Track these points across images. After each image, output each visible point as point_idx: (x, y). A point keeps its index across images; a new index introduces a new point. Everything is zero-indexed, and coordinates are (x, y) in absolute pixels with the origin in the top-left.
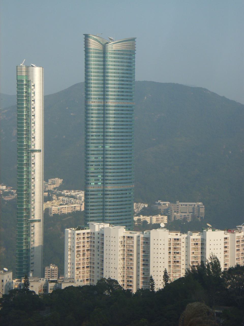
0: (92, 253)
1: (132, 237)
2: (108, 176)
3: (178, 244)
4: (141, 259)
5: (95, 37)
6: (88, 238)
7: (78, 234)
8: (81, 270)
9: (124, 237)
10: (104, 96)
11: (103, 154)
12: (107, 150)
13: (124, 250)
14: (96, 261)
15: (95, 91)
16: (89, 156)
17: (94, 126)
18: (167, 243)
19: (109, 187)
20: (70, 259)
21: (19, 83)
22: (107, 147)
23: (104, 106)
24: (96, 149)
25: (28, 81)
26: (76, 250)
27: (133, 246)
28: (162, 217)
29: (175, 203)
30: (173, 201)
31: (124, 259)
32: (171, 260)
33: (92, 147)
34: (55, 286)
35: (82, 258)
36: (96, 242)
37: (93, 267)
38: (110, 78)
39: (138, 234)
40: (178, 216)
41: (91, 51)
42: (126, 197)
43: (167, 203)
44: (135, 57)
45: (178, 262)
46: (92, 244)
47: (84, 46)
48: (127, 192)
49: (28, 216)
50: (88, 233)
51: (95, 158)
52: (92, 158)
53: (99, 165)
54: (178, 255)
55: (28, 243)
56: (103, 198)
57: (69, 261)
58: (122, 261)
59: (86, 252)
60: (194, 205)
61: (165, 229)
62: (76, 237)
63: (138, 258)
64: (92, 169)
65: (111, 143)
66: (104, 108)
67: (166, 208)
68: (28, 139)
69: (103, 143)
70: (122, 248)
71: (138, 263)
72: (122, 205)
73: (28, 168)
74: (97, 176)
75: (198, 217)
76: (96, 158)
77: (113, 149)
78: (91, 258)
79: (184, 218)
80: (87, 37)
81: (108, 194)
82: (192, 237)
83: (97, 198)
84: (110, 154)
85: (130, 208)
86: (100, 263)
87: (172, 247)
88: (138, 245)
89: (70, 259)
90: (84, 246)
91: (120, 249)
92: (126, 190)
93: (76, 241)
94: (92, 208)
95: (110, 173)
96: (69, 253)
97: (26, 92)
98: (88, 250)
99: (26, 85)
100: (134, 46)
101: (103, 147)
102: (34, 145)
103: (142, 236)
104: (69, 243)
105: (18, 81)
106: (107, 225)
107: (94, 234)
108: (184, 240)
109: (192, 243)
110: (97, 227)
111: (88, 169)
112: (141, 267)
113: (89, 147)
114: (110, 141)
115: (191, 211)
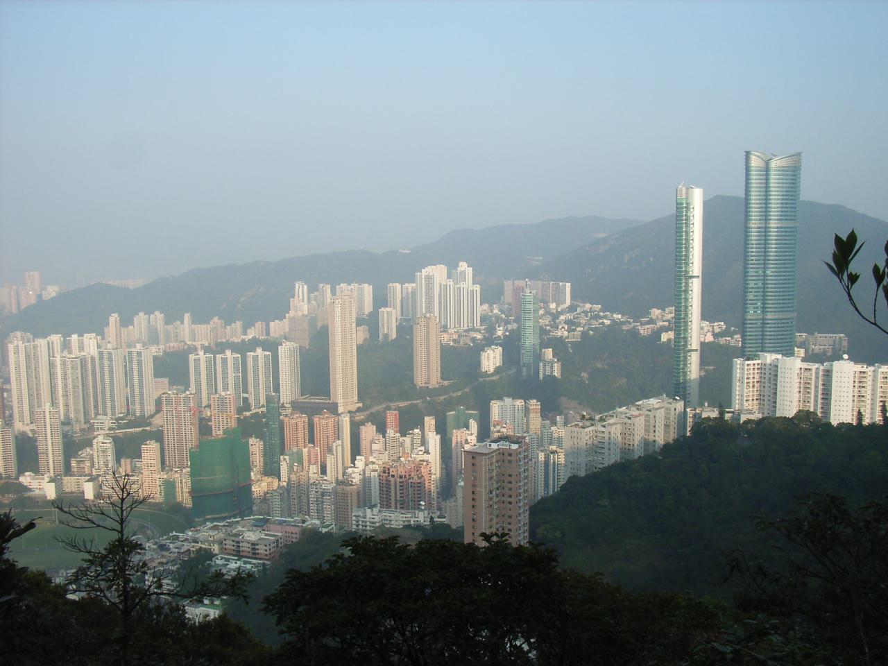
0: (762, 385)
1: (810, 369)
2: (768, 304)
3: (865, 377)
4: (820, 392)
5: (757, 154)
6: (758, 369)
7: (748, 365)
8: (750, 402)
9: (801, 369)
10: (765, 217)
11: (764, 280)
12: (768, 276)
13: (800, 383)
14: (766, 394)
15: (756, 212)
16: (747, 282)
17: (773, 246)
18: (852, 376)
19: (769, 316)
20: (739, 391)
21: (679, 206)
22: (768, 272)
23: (766, 228)
24: (757, 274)
25: (688, 204)
26: (746, 381)
27: (811, 379)
28: (798, 349)
29: (813, 334)
30: (810, 333)
31: (800, 392)
32: (856, 394)
33: (751, 272)
34: (732, 417)
35: (751, 389)
36: (767, 374)
37: (764, 400)
38: (772, 197)
39: (817, 365)
40: (817, 349)
41: (752, 169)
42: (788, 327)
43: (804, 335)
44: (800, 174)
45: (863, 396)
46: (763, 376)
47: (745, 160)
48: (790, 321)
49: (685, 346)
50: (758, 364)
51: (756, 284)
52: (752, 284)
53: (759, 292)
54: (863, 389)
55: (685, 373)
56: (763, 327)
57: (737, 393)
58: (797, 395)
59: (756, 384)
60: (836, 337)
61: (849, 361)
62: (746, 367)
63: (816, 391)
64: (751, 296)
65: (772, 268)
66: (765, 231)
67: (803, 340)
68: (687, 264)
69: (764, 268)
70: (799, 381)
71: (816, 396)
72: (783, 335)
73: (686, 295)
74: (756, 304)
75: (840, 350)
76: (756, 284)
77: (775, 274)
78: (760, 390)
79: (823, 352)
80: (748, 154)
81: (768, 324)
82: (880, 370)
83: (756, 328)
84: (772, 280)
85: (791, 338)
86: (772, 396)
87: (856, 380)
88: (817, 378)
89: (739, 391)
90: (754, 378)
91: (796, 381)
92: (788, 319)
93: (746, 372)
94: (750, 337)
95: (771, 300)
96: (738, 384)
97: (686, 215)
98: (757, 382)
99: (686, 207)
100: (799, 161)
101: (764, 272)
102: (692, 271)
103: (822, 368)
104: (737, 374)
105: (677, 204)
106: (779, 356)
107: (765, 365)
108: (870, 373)
109: (880, 376)
110: (769, 358)
111: (746, 296)
112: (820, 401)
113: (748, 272)
114: (772, 266)
115: (831, 343)
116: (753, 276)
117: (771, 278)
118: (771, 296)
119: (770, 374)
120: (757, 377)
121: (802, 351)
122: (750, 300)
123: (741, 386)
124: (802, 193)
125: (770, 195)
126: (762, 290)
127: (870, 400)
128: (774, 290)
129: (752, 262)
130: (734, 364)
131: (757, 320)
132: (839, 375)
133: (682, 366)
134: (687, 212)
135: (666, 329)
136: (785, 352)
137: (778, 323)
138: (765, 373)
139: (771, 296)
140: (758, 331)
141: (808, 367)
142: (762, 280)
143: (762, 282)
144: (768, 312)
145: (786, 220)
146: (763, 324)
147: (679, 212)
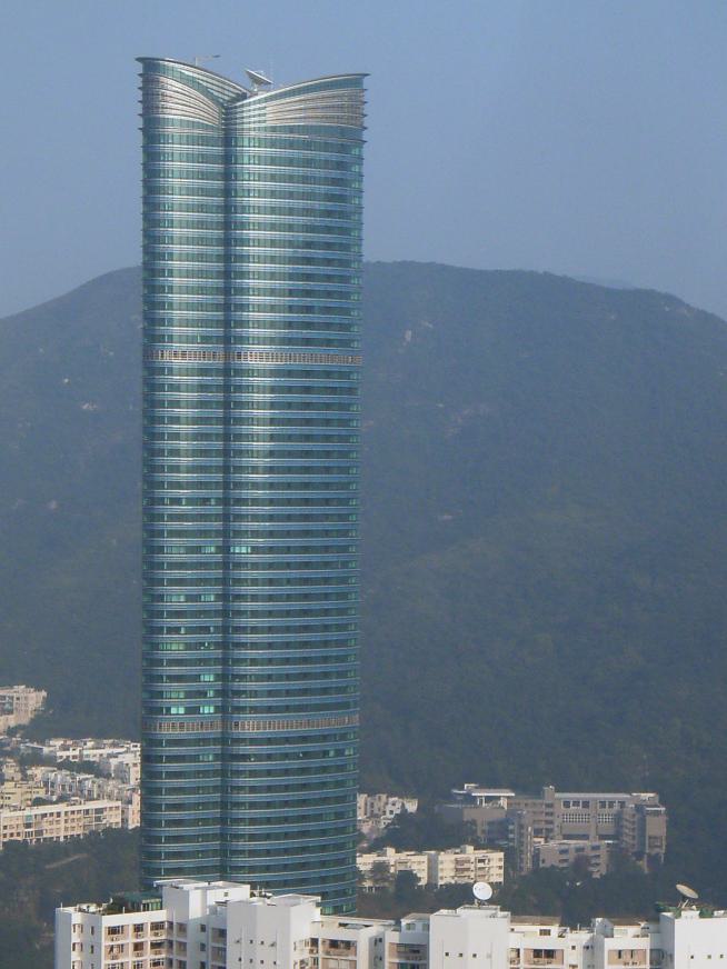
1: (348, 945)
5: (188, 72)
6: (155, 945)
7: (113, 931)
9: (314, 942)
10: (227, 328)
11: (224, 581)
12: (238, 565)
15: (189, 306)
16: (159, 589)
19: (250, 726)
22: (241, 550)
23: (226, 371)
24: (194, 557)
28: (481, 854)
29: (538, 793)
30: (528, 787)
33: (175, 550)
39: (376, 928)
40: (552, 850)
41: (170, 130)
42: (324, 769)
43: (504, 795)
44: (361, 158)
48: (329, 746)
50: (157, 926)
51: (190, 598)
52: (176, 598)
53: (206, 629)
56: (223, 773)
60: (622, 804)
61: (495, 909)
62: (105, 942)
64: (174, 646)
65: (256, 534)
66: (226, 382)
67: (499, 815)
69: (225, 533)
74: (196, 678)
75: (639, 855)
76: (190, 598)
77: (268, 558)
80: (151, 70)
81: (245, 757)
82: (610, 944)
83: (197, 774)
92: (325, 738)
94: (176, 814)
95: (254, 662)
100: (356, 109)
101: (225, 549)
103: (392, 937)
106: (240, 893)
110: (198, 899)
111: (155, 646)
113: (161, 549)
115: (609, 828)
116: (181, 566)
117: (255, 574)
119: (203, 947)
121: (496, 859)
122: (173, 662)
124: (369, 235)
125: (244, 242)
126: (219, 621)
130: (60, 926)
131: (204, 741)
139: (254, 646)
140: (205, 789)
141: (343, 935)
143: (219, 588)
145: (308, 342)
146: (226, 757)
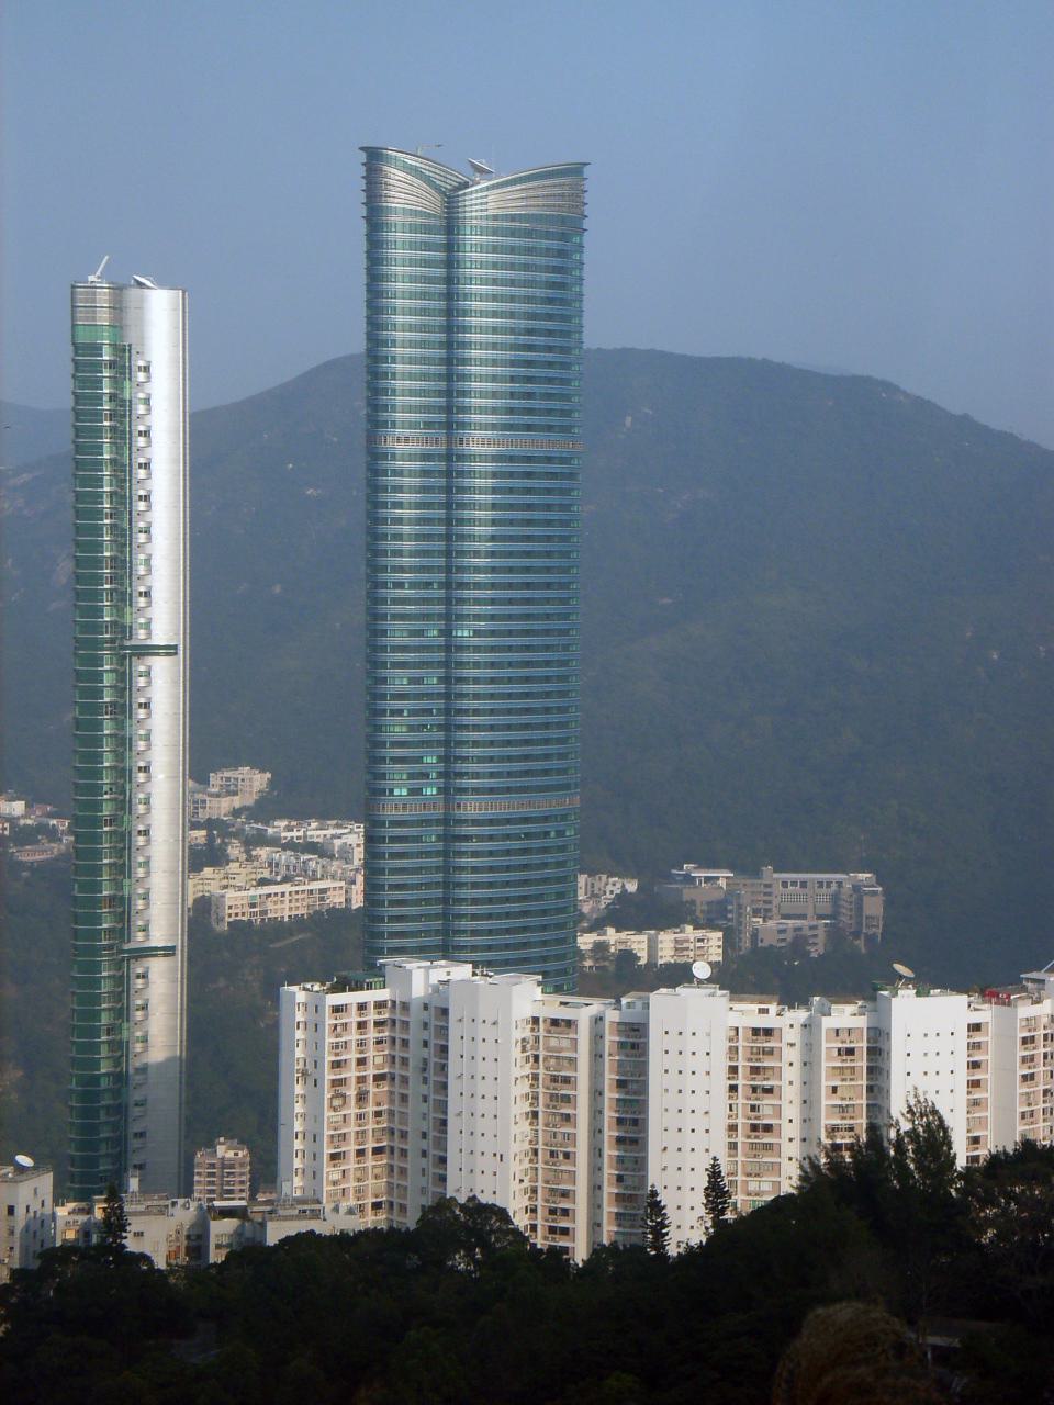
1: (569, 1023)
3: (770, 1052)
4: (609, 1114)
5: (411, 161)
6: (378, 1024)
7: (337, 1009)
8: (351, 1164)
9: (536, 1020)
10: (449, 414)
11: (446, 664)
12: (461, 648)
13: (535, 1077)
14: (413, 1126)
15: (412, 393)
16: (383, 672)
18: (720, 1047)
19: (471, 807)
21: (84, 358)
22: (463, 633)
23: (449, 457)
24: (415, 641)
25: (122, 350)
26: (329, 1076)
27: (573, 1061)
28: (700, 933)
29: (757, 873)
30: (746, 867)
31: (535, 1114)
32: (740, 1121)
33: (397, 633)
35: (352, 1110)
38: (474, 337)
39: (596, 1006)
40: (769, 929)
41: (393, 218)
42: (545, 850)
43: (723, 875)
45: (768, 1128)
46: (398, 1053)
47: (363, 197)
48: (549, 826)
49: (122, 931)
50: (380, 1005)
51: (413, 681)
52: (399, 681)
53: (428, 712)
54: (768, 1101)
55: (120, 1048)
56: (445, 854)
57: (298, 1126)
59: (371, 1087)
60: (840, 884)
61: (714, 988)
62: (329, 1021)
63: (596, 1112)
64: (397, 729)
65: (477, 617)
66: (449, 467)
67: (718, 895)
68: (123, 598)
69: (447, 617)
70: (528, 1070)
71: (596, 1131)
73: (120, 725)
74: (419, 760)
75: (857, 935)
76: (413, 681)
77: (490, 641)
78: (391, 1113)
80: (374, 159)
81: (467, 838)
82: (828, 1023)
83: (420, 854)
87: (742, 1063)
88: (597, 1056)
89: (304, 1116)
90: (361, 1062)
92: (546, 819)
93: (329, 1040)
95: (476, 744)
96: (299, 1089)
97: (113, 397)
98: (378, 1078)
99: (112, 364)
100: (577, 197)
101: (447, 632)
102: (147, 626)
103: (612, 1016)
104: (297, 1048)
105: (77, 347)
106: (463, 972)
107: (405, 1006)
109: (827, 1045)
110: (421, 977)
112: (610, 1151)
113: (384, 633)
115: (827, 908)
118: (476, 728)
120: (377, 1059)
121: (715, 938)
123: (312, 1100)
127: (797, 1142)
128: (490, 688)
129: (400, 593)
132: (672, 1043)
133: (105, 1019)
134: (117, 382)
135: (73, 1262)
136: (551, 966)
137: (508, 837)
138: (405, 1043)
139: (476, 728)
140: (427, 869)
142: (439, 664)
143: (441, 671)
144: (463, 791)
147: (85, 481)
